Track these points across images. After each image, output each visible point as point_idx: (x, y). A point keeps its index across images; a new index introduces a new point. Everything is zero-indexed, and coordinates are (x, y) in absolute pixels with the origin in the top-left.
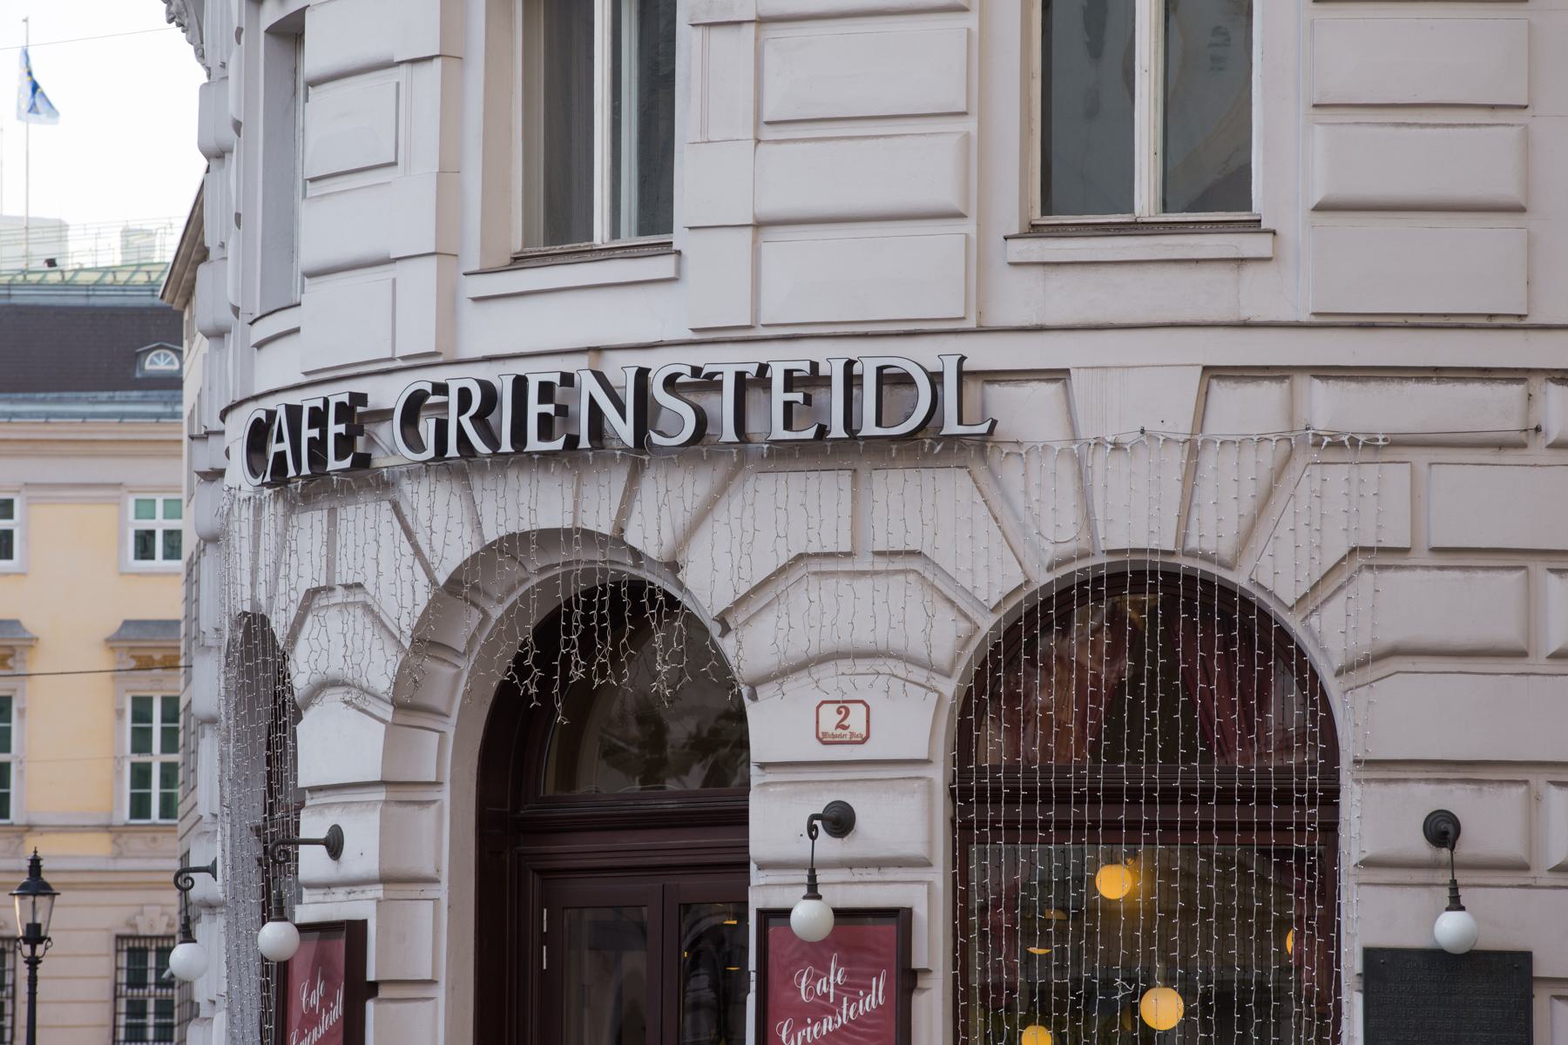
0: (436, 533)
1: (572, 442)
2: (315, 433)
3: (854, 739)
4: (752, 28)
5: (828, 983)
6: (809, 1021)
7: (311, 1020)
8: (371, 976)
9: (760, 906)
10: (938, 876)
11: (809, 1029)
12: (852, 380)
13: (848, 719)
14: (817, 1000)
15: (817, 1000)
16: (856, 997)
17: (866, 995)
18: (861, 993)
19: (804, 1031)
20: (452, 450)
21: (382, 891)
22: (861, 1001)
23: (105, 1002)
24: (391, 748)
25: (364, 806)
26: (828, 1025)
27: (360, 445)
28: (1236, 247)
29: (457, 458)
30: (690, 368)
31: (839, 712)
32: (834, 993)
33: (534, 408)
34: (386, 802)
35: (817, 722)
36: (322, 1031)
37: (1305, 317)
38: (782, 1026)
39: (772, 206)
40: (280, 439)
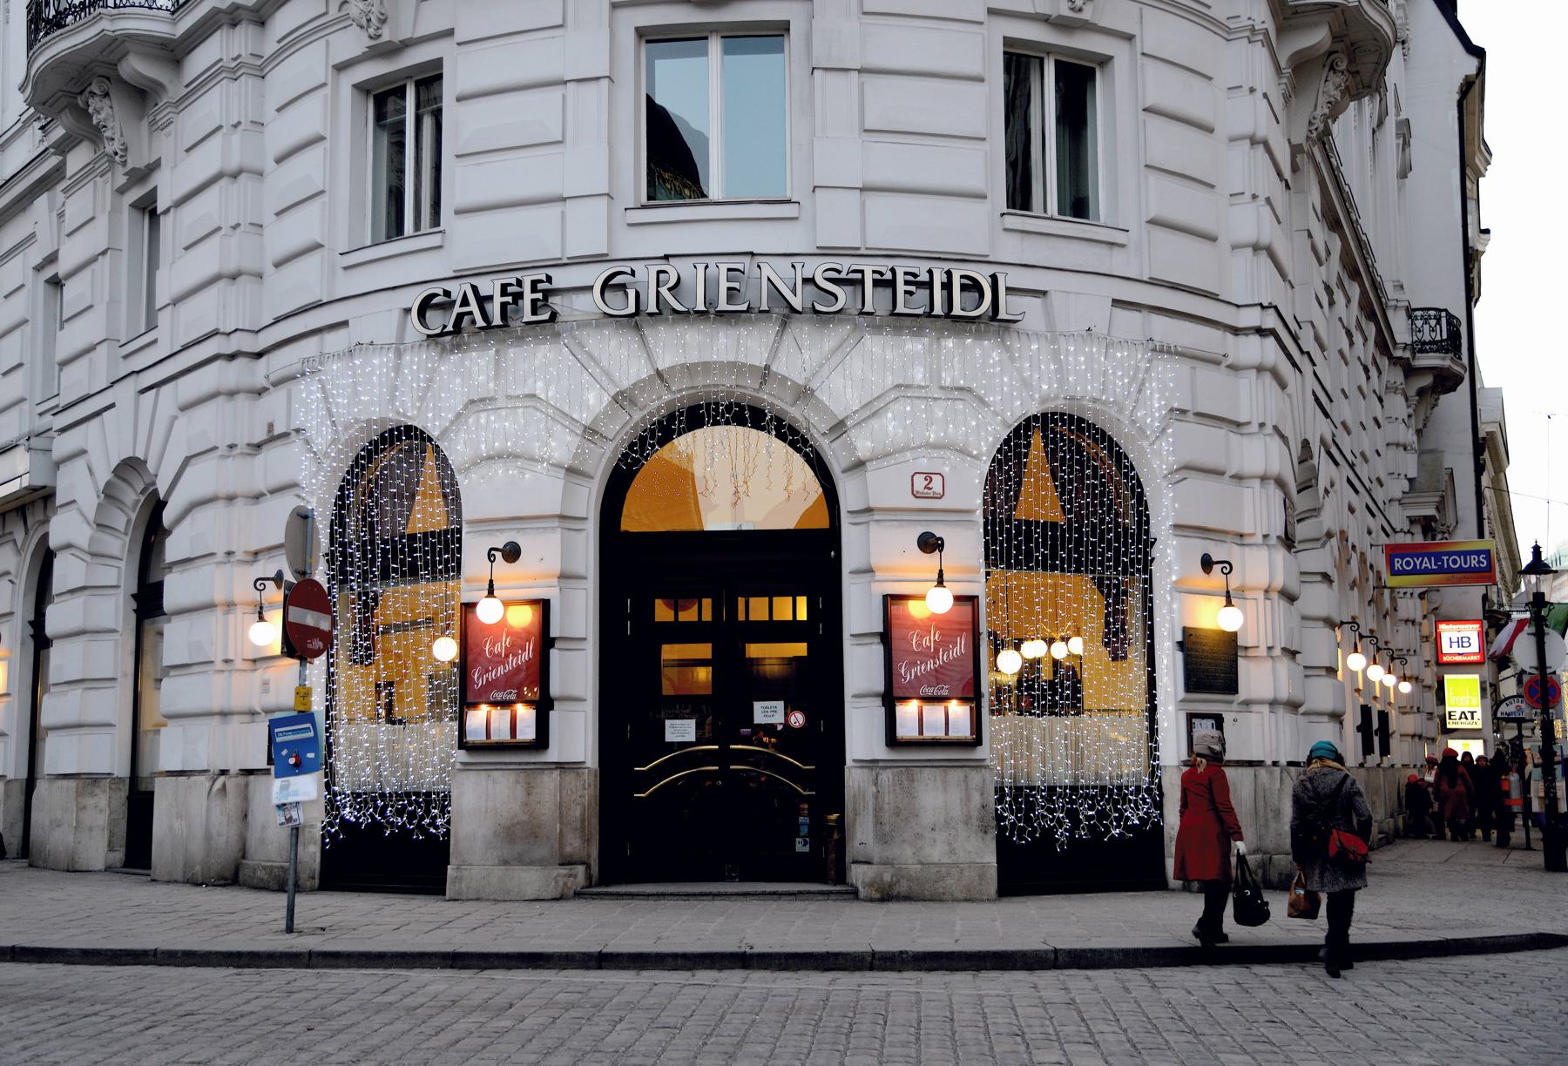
0: (271, 426)
17: (953, 648)
24: (566, 495)
26: (930, 665)
37: (1146, 279)
39: (875, 178)
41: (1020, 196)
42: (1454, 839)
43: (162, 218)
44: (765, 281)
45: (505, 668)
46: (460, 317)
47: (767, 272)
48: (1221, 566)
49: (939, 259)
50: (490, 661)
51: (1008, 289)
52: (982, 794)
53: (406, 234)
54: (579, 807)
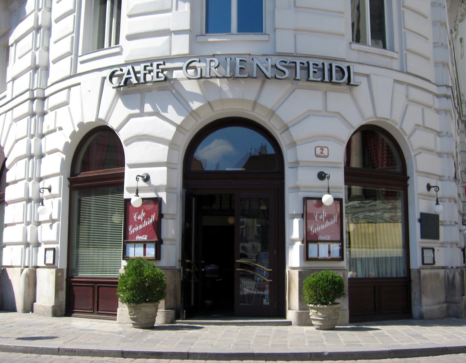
5: (323, 216)
6: (318, 226)
11: (318, 228)
17: (332, 219)
18: (331, 219)
23: (14, 221)
26: (141, 227)
29: (180, 80)
31: (321, 149)
38: (311, 227)
41: (357, 38)
43: (10, 47)
44: (255, 66)
45: (324, 226)
46: (127, 79)
47: (256, 61)
48: (434, 188)
49: (326, 59)
51: (354, 73)
53: (105, 47)
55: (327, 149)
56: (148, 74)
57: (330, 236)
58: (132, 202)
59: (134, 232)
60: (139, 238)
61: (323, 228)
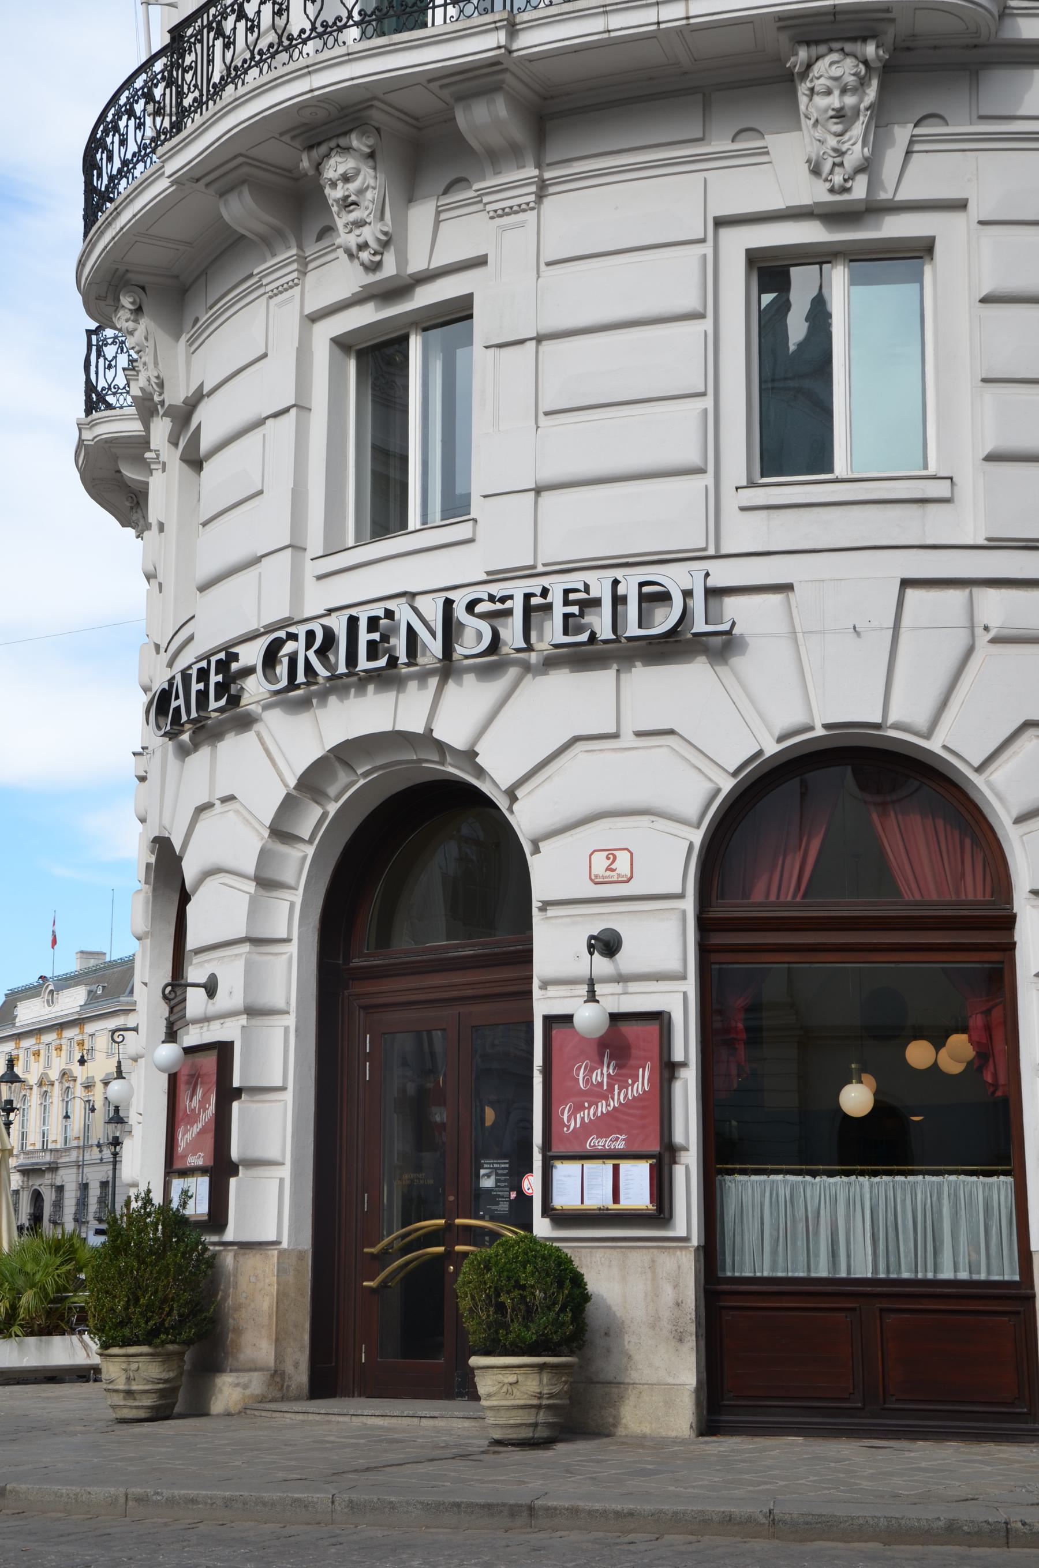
1: (393, 661)
2: (201, 686)
3: (620, 879)
4: (534, 343)
5: (602, 1073)
6: (586, 1105)
7: (192, 1119)
8: (236, 1083)
9: (546, 1013)
10: (690, 986)
11: (586, 1111)
12: (618, 600)
13: (616, 863)
14: (593, 1088)
15: (593, 1088)
16: (626, 1085)
18: (630, 1081)
19: (582, 1113)
20: (301, 678)
21: (246, 1020)
22: (630, 1088)
24: (254, 909)
25: (233, 958)
26: (602, 1108)
27: (234, 689)
28: (922, 490)
30: (487, 594)
31: (608, 858)
32: (607, 1082)
33: (364, 636)
34: (249, 953)
35: (590, 867)
36: (200, 1126)
37: (981, 541)
38: (564, 1109)
39: (550, 473)
40: (177, 697)
42: (358, 1397)
45: (608, 1105)
50: (582, 1093)
52: (676, 1286)
53: (411, 527)
54: (267, 1298)
55: (629, 854)
56: (382, 619)
57: (623, 1137)
58: (576, 1020)
59: (578, 1125)
60: (596, 1143)
61: (604, 1112)
